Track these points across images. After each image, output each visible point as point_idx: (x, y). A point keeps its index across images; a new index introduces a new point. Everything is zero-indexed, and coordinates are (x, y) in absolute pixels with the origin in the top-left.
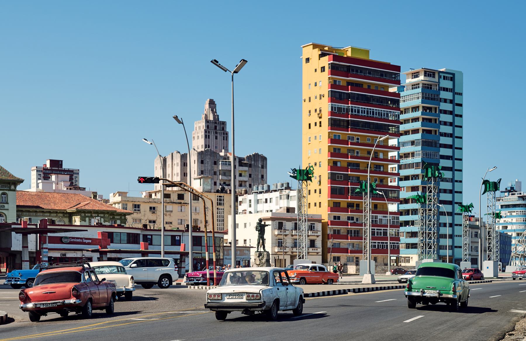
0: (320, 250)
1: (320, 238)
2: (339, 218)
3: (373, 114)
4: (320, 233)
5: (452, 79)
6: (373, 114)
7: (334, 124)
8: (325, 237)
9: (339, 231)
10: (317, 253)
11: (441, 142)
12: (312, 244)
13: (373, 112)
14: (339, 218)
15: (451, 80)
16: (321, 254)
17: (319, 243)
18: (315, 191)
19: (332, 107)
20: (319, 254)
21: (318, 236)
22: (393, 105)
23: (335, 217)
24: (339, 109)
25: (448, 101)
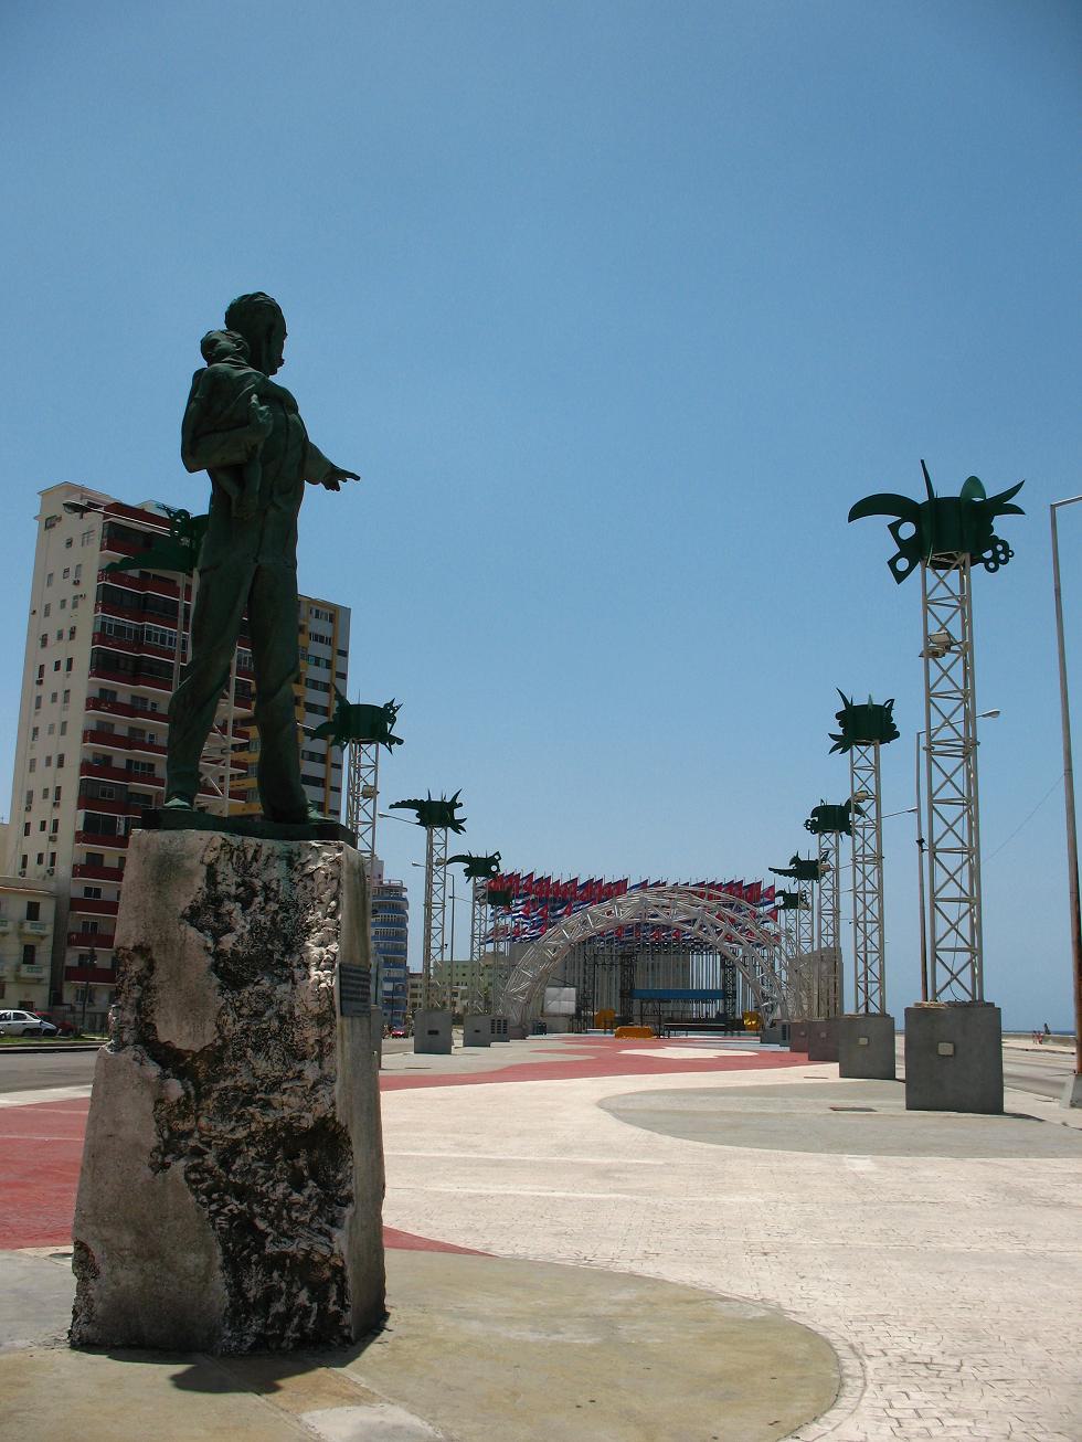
0: (46, 973)
1: (49, 942)
2: (98, 891)
3: (163, 642)
4: (49, 930)
5: (332, 619)
6: (163, 642)
7: (103, 665)
8: (62, 940)
9: (95, 925)
10: (39, 980)
11: (303, 772)
12: (29, 955)
13: (163, 637)
14: (98, 891)
15: (331, 621)
16: (48, 981)
17: (44, 952)
18: (43, 823)
19: (103, 624)
20: (44, 982)
21: (43, 937)
22: (442, 962)
23: (88, 891)
24: (120, 630)
25: (317, 758)
